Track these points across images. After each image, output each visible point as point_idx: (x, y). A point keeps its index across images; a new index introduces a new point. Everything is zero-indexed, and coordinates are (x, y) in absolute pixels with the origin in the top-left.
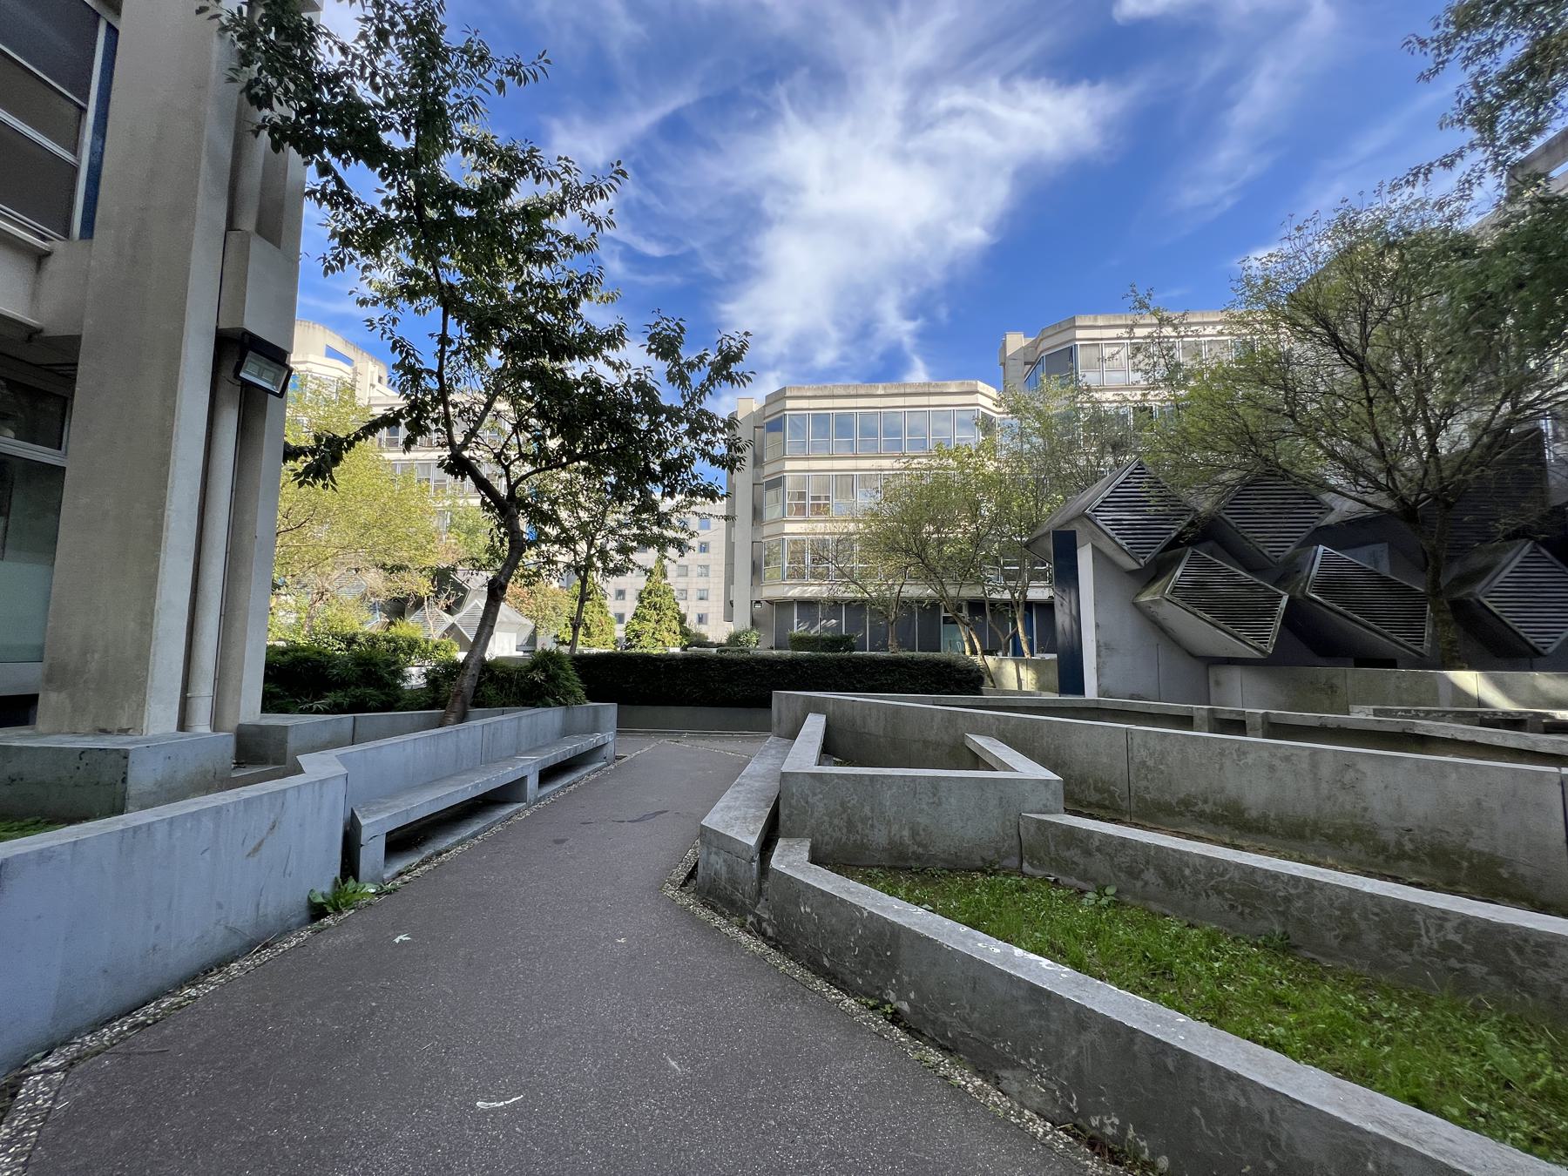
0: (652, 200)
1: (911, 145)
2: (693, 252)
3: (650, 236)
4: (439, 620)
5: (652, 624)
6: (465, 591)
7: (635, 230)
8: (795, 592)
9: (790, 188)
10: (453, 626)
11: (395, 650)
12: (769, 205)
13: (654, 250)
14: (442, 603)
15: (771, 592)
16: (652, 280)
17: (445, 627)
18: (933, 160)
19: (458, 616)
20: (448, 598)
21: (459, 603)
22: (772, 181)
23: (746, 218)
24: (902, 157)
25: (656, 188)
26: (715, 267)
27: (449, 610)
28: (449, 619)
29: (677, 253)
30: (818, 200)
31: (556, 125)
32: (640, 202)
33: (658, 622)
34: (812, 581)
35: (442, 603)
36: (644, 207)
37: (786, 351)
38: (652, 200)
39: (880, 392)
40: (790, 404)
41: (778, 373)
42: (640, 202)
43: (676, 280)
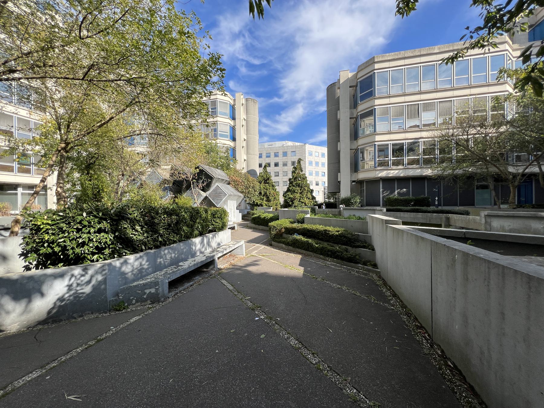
0: (256, 43)
1: (354, 6)
2: (271, 61)
3: (255, 57)
4: (199, 195)
5: (298, 195)
6: (211, 178)
7: (250, 55)
8: (383, 174)
9: (305, 31)
10: (206, 197)
11: (177, 223)
12: (298, 39)
13: (257, 62)
14: (200, 185)
15: (362, 176)
16: (257, 73)
17: (202, 198)
18: (363, 11)
19: (208, 193)
20: (203, 183)
21: (208, 186)
22: (299, 29)
23: (290, 44)
24: (350, 12)
25: (255, 38)
26: (278, 66)
27: (204, 190)
28: (204, 194)
29: (265, 62)
30: (317, 35)
31: (221, 18)
32: (251, 44)
33: (301, 193)
34: (394, 167)
35: (200, 185)
36: (252, 46)
37: (305, 95)
38: (256, 43)
39: (436, 51)
40: (377, 66)
41: (302, 104)
42: (251, 44)
43: (265, 72)
